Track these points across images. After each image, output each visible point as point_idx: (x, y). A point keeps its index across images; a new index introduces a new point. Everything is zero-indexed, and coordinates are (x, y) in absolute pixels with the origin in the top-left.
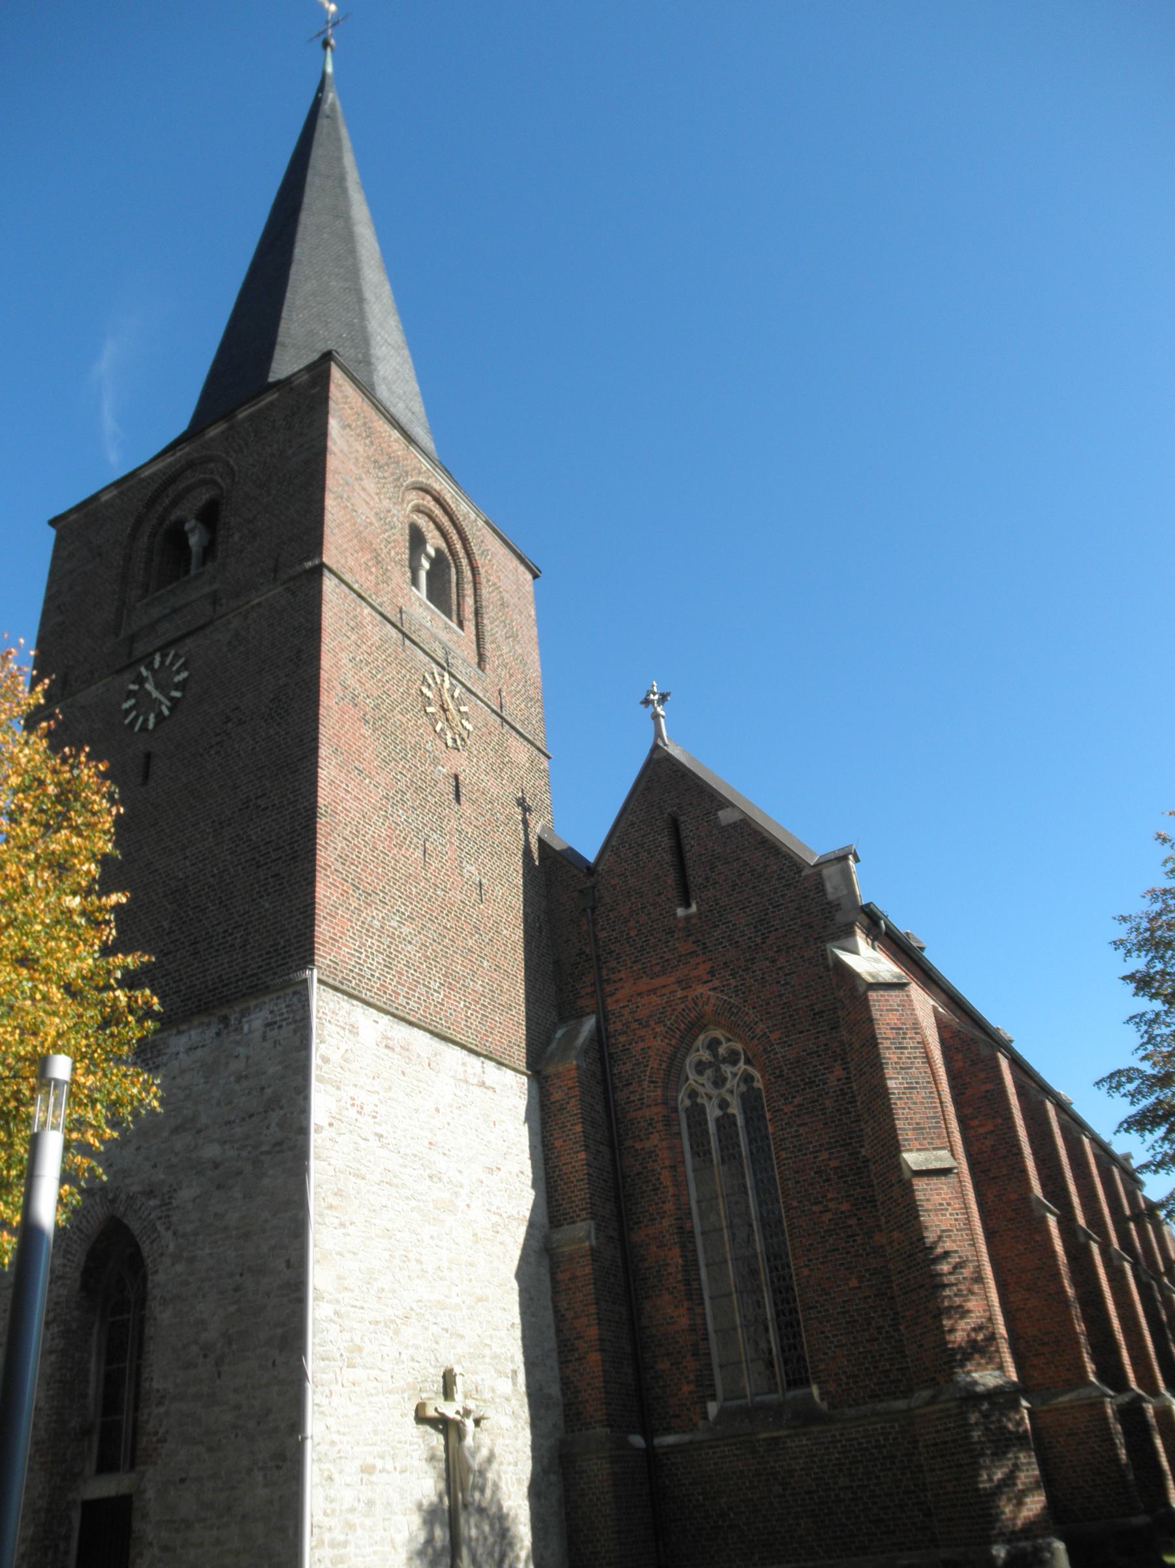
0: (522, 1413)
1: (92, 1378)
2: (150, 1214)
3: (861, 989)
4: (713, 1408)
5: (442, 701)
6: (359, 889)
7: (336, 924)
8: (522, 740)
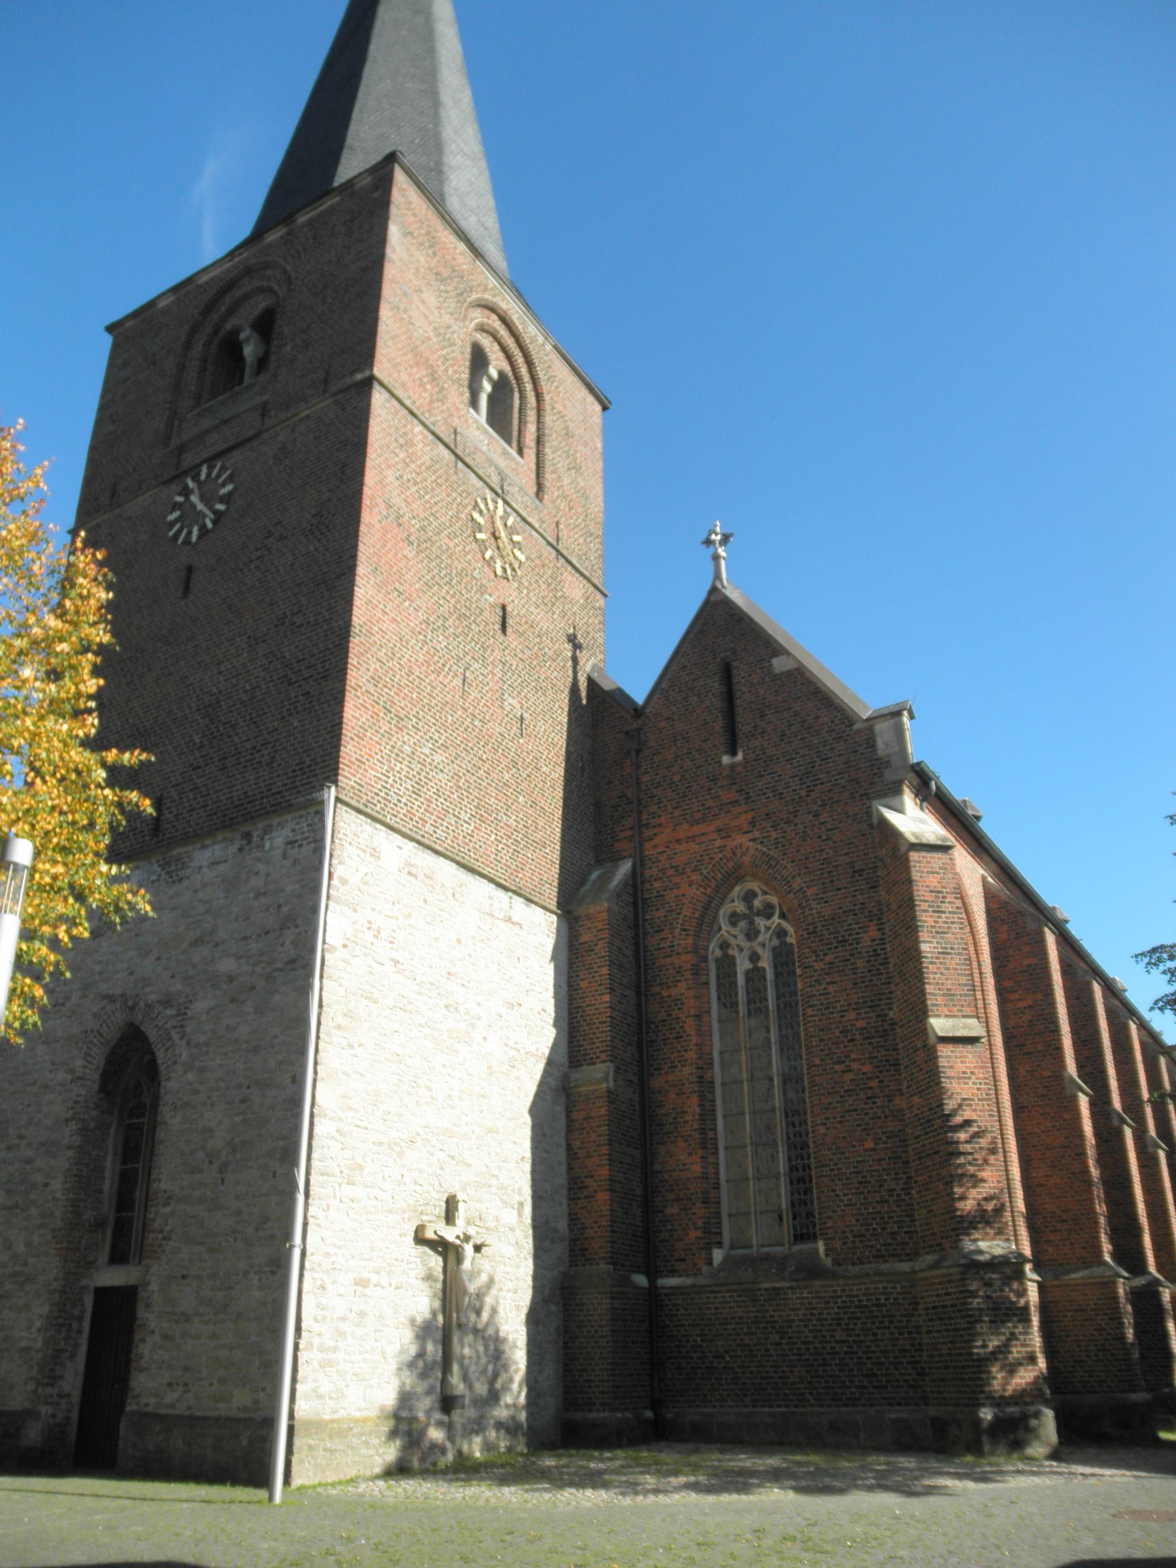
0: (526, 1245)
1: (108, 1175)
2: (166, 1023)
3: (903, 849)
4: (718, 1255)
5: (494, 528)
6: (390, 712)
7: (364, 746)
8: (578, 575)
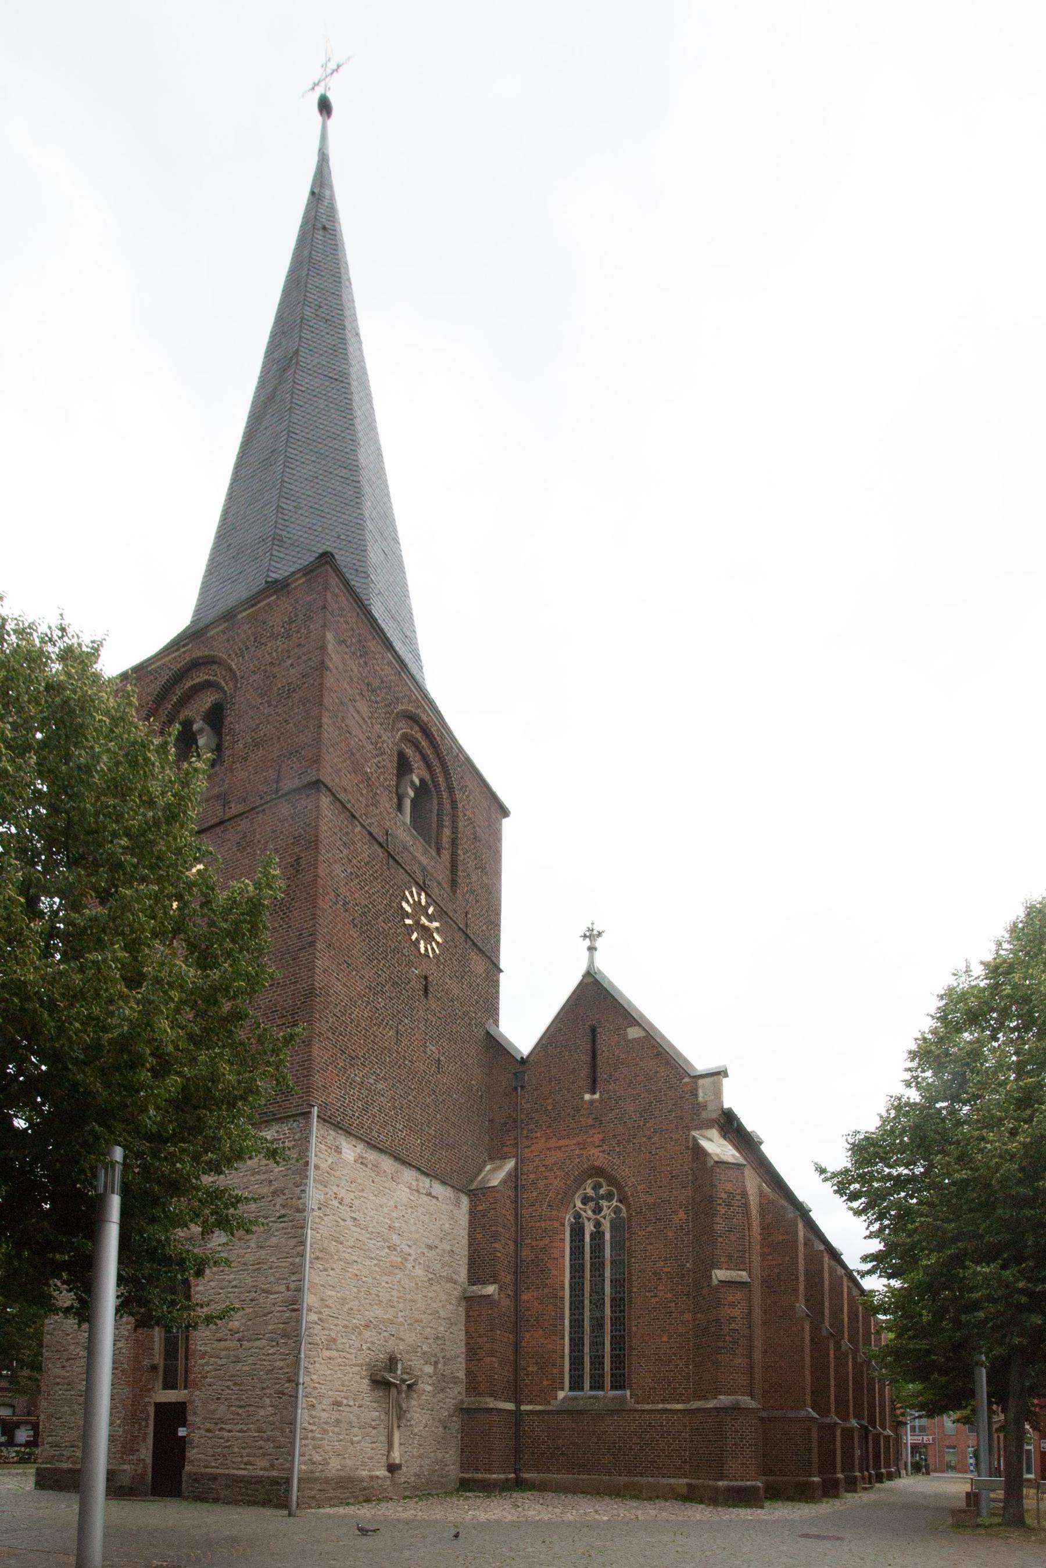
6: (345, 1053)
